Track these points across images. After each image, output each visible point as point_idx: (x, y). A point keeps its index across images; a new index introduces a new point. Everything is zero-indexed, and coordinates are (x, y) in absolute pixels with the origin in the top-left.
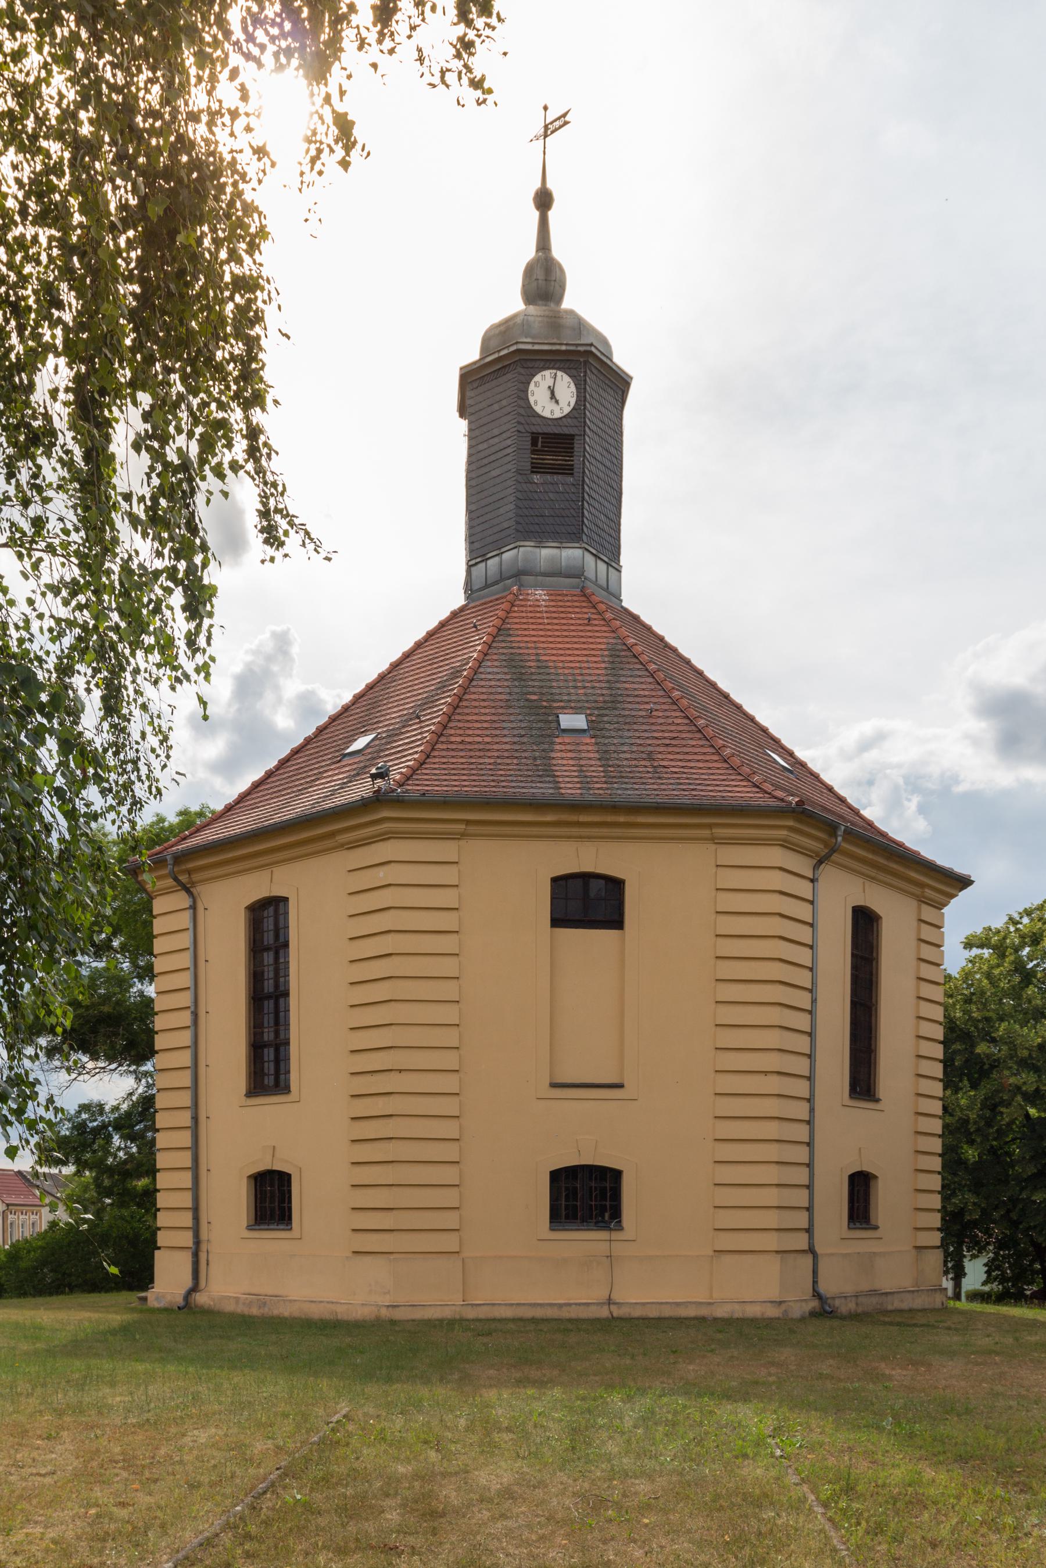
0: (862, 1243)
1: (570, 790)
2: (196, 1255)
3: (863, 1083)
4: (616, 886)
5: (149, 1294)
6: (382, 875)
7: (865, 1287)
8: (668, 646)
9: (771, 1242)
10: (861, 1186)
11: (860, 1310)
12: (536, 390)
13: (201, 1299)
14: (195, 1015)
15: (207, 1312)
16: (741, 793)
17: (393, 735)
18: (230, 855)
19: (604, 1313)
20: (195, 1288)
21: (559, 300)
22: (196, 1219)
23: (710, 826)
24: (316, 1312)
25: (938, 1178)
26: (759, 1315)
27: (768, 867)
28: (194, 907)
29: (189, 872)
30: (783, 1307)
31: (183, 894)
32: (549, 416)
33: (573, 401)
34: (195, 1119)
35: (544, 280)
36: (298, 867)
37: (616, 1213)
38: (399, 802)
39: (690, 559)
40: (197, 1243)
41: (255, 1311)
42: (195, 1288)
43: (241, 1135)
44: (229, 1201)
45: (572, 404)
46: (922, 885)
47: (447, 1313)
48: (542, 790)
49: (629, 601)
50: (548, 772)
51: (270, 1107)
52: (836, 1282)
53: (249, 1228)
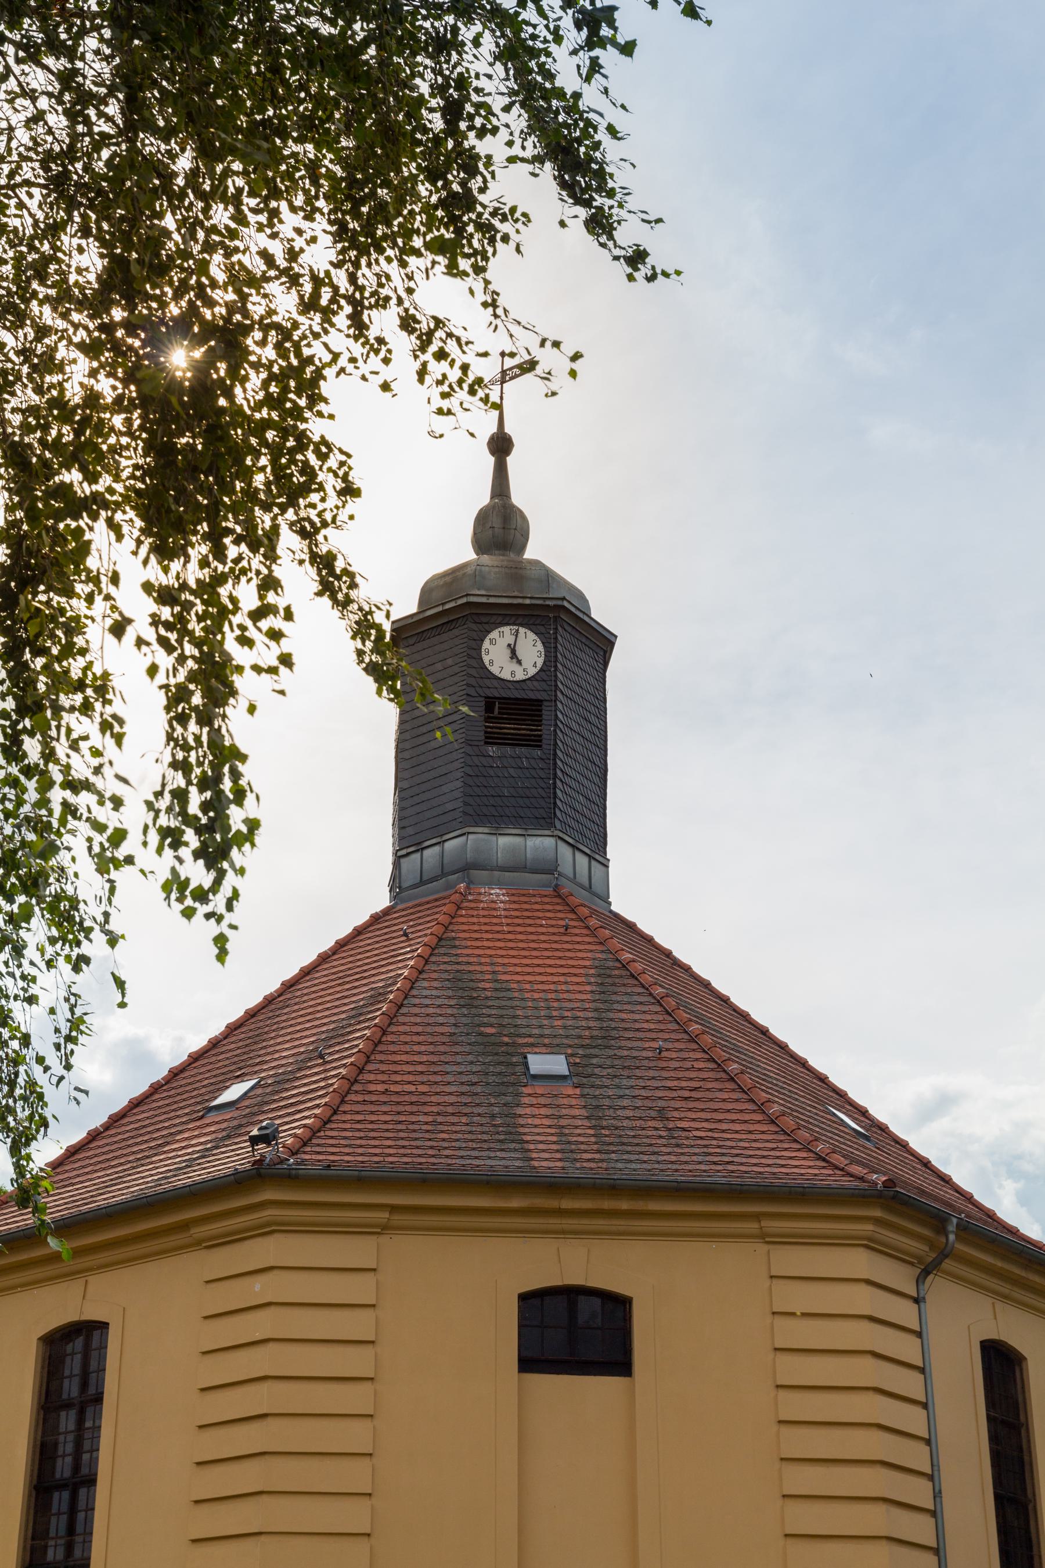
1: (546, 1161)
4: (617, 1306)
6: (258, 1289)
12: (491, 648)
23: (757, 1217)
27: (847, 1279)
32: (508, 677)
33: (540, 662)
35: (500, 527)
38: (291, 1178)
39: (706, 856)
45: (539, 665)
48: (503, 1161)
50: (512, 1135)
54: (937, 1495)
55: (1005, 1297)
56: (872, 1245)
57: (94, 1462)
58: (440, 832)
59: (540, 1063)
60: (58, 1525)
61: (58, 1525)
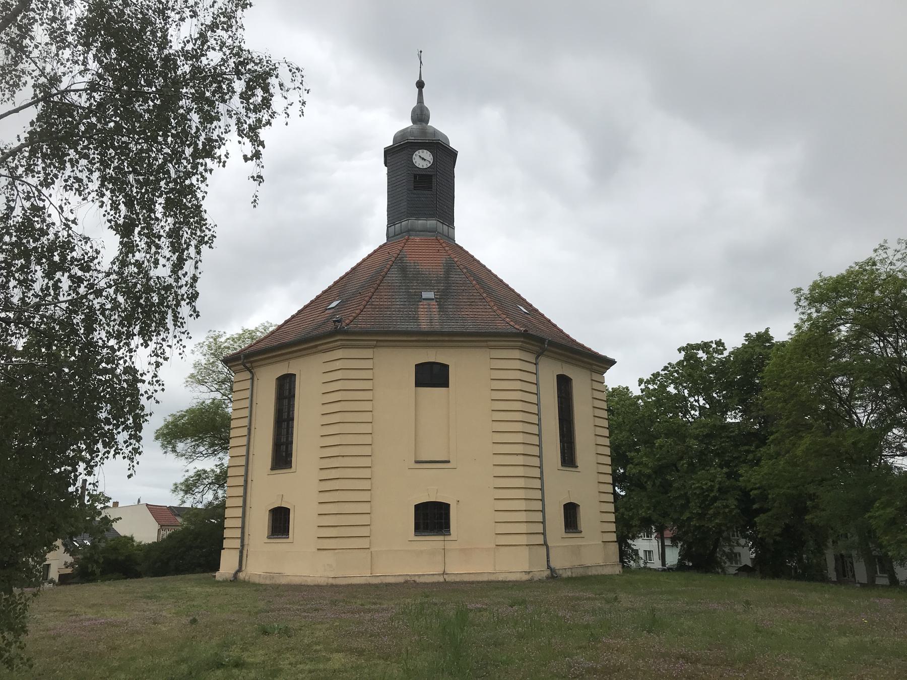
0: (573, 541)
1: (424, 326)
2: (241, 552)
3: (568, 458)
4: (445, 367)
5: (217, 574)
6: (338, 364)
7: (577, 563)
8: (475, 260)
9: (523, 540)
10: (571, 512)
11: (574, 575)
13: (241, 576)
14: (249, 430)
15: (246, 584)
16: (501, 326)
17: (347, 300)
18: (274, 354)
19: (441, 579)
20: (240, 570)
21: (427, 122)
22: (243, 533)
23: (486, 341)
24: (297, 581)
25: (612, 506)
26: (518, 579)
28: (252, 379)
29: (251, 362)
30: (531, 574)
31: (248, 372)
34: (246, 481)
35: (420, 115)
36: (301, 360)
37: (447, 526)
38: (346, 333)
39: (485, 227)
40: (243, 546)
41: (268, 582)
42: (240, 570)
43: (269, 489)
44: (259, 522)
46: (592, 364)
47: (361, 581)
48: (411, 327)
49: (458, 241)
50: (416, 319)
51: (283, 476)
52: (560, 562)
53: (268, 538)
54: (540, 420)
55: (566, 362)
56: (521, 349)
57: (293, 414)
58: (400, 220)
59: (425, 295)
60: (284, 432)
61: (284, 432)
